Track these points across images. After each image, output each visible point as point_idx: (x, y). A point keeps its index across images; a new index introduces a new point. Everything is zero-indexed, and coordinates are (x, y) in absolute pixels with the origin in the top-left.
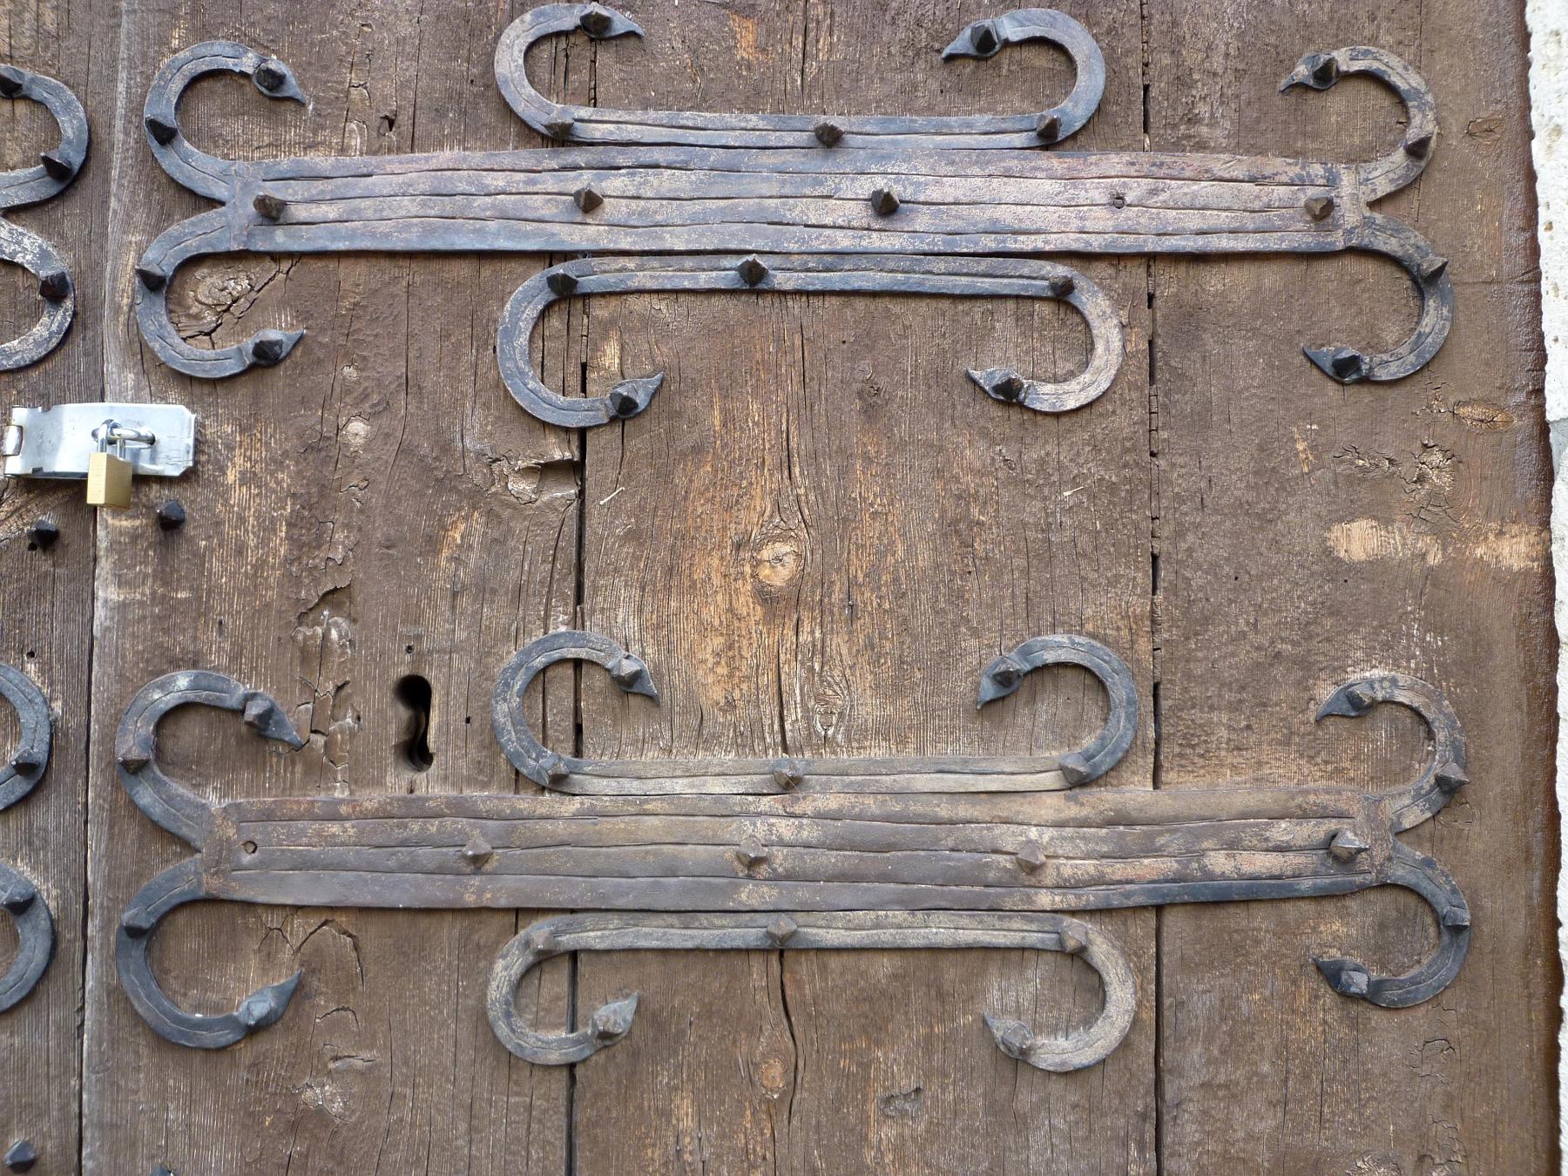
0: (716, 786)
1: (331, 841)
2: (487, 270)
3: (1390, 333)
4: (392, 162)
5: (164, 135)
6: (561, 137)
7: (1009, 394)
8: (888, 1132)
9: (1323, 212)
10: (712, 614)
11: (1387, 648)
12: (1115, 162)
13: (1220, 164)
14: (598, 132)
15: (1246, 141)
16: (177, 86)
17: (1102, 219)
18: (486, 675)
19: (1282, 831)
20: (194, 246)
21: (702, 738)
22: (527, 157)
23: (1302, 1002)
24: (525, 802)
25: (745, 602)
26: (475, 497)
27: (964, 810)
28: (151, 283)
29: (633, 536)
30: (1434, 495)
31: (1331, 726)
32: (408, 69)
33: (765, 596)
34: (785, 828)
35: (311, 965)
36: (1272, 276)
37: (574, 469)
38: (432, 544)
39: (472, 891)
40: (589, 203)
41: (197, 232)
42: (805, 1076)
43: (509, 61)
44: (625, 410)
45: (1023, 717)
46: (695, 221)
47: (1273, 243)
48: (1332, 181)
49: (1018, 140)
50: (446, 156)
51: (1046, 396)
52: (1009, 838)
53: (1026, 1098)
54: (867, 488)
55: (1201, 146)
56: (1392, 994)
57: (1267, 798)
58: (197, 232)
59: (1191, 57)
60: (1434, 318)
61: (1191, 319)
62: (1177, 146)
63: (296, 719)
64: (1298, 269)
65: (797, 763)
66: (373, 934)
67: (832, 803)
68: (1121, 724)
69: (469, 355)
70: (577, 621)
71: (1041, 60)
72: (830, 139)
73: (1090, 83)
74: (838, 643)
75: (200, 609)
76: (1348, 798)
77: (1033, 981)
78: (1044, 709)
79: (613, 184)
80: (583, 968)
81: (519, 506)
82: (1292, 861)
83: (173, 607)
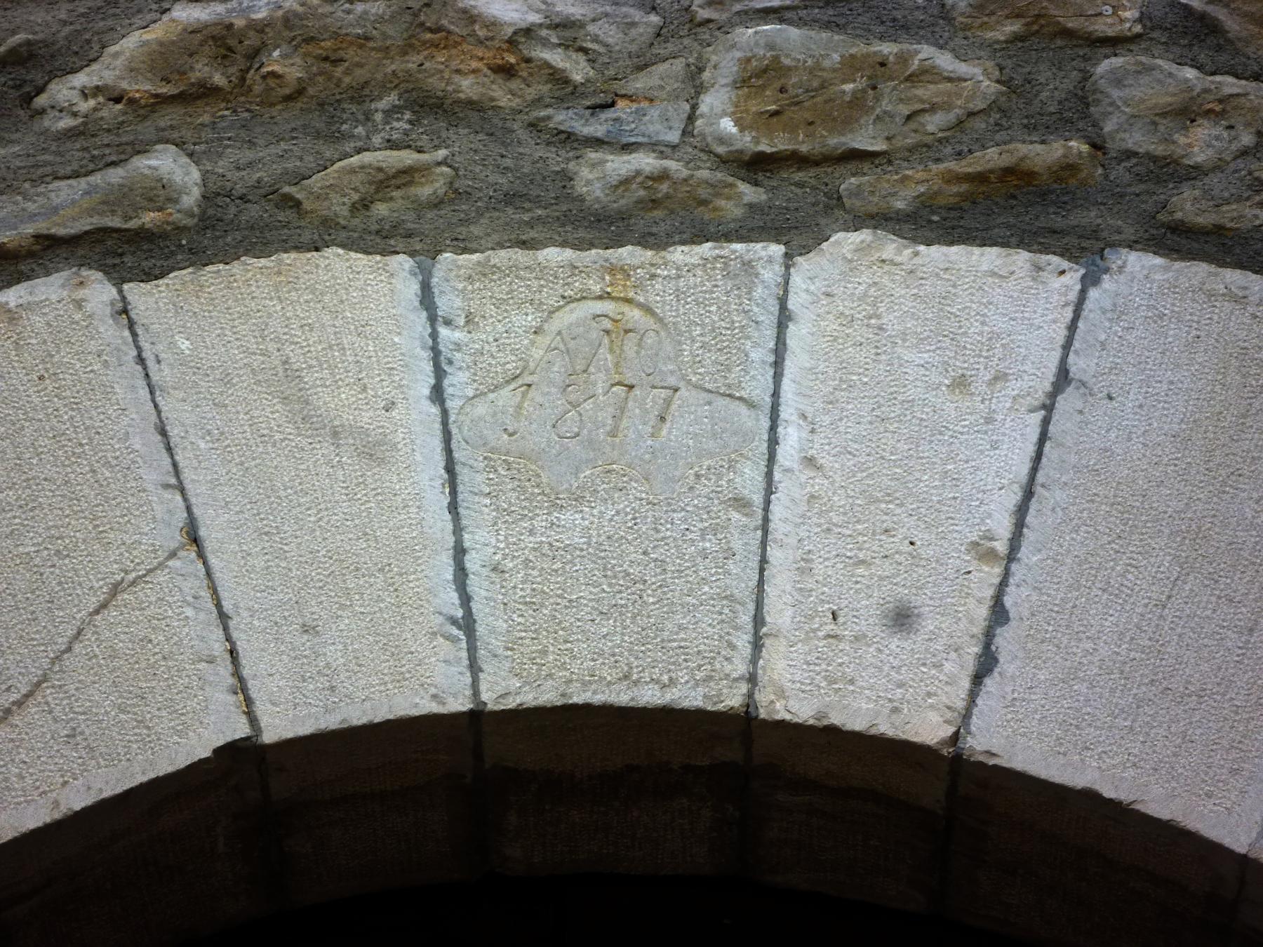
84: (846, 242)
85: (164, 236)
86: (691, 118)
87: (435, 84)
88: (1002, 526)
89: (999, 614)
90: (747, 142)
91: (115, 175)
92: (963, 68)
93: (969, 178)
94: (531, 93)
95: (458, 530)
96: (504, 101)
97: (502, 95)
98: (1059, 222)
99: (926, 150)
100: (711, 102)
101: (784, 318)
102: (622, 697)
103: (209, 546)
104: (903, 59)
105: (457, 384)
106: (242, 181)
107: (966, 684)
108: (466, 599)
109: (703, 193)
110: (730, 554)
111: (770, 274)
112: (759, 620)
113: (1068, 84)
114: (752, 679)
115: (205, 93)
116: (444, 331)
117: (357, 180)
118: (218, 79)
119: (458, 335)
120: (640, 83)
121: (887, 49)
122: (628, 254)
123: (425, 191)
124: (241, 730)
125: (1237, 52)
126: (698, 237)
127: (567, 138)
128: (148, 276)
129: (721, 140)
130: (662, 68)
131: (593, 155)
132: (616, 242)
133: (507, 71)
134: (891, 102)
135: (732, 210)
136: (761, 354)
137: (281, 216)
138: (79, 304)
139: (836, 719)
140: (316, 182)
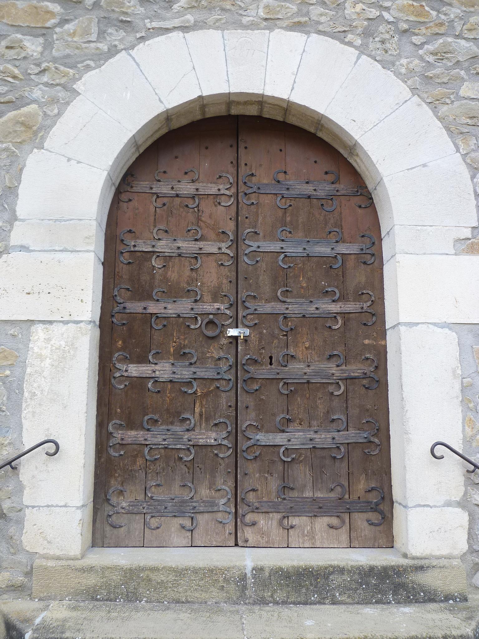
0: (301, 366)
1: (264, 372)
2: (277, 315)
3: (370, 320)
4: (268, 304)
5: (244, 302)
6: (284, 302)
7: (330, 327)
8: (319, 401)
9: (362, 308)
10: (300, 349)
11: (370, 353)
12: (341, 303)
13: (351, 303)
14: (288, 301)
15: (354, 301)
16: (245, 296)
17: (339, 309)
18: (278, 355)
19: (359, 371)
20: (248, 313)
21: (300, 362)
22: (281, 304)
23: (362, 389)
24: (283, 368)
25: (304, 348)
26: (277, 338)
27: (326, 369)
28: (244, 317)
29: (293, 342)
30: (375, 337)
31: (364, 361)
32: (268, 294)
33: (306, 348)
34: (308, 370)
35: (262, 385)
36: (357, 315)
37: (286, 335)
38: (273, 343)
39: (278, 377)
40: (287, 309)
41: (248, 311)
42: (311, 396)
43: (279, 294)
44: (292, 329)
45: (332, 360)
46: (298, 310)
47: (357, 311)
48: (363, 305)
49: (330, 301)
50: (273, 303)
51: (334, 327)
52: (331, 372)
53: (333, 398)
54: (316, 337)
55: (350, 301)
56: (370, 388)
57: (357, 368)
58: (248, 311)
59: (348, 292)
60: (374, 319)
61: (349, 319)
62: (347, 301)
63: (260, 360)
64: (21, 452)
65: (309, 364)
66: (268, 381)
67: (313, 368)
68: (342, 360)
69: (276, 324)
70: (287, 350)
71: (333, 293)
72: (311, 302)
73: (338, 295)
74: (313, 352)
75: (249, 349)
76: (366, 368)
77: (334, 386)
78: (334, 359)
79: (290, 306)
80: (289, 385)
81: (281, 339)
82: (360, 374)
83: (246, 349)
84: (277, 31)
85: (189, 27)
86: (257, 13)
87: (224, 7)
88: (296, 70)
89: (295, 82)
90: (265, 16)
91: (182, 18)
92: (293, 7)
93: (293, 22)
94: (236, 8)
95: (227, 69)
96: (233, 9)
97: (233, 8)
98: (304, 29)
99: (288, 18)
100: (259, 10)
101: (269, 41)
102: (248, 91)
103: (196, 69)
104: (285, 5)
105: (227, 48)
106: (199, 20)
107: (290, 91)
108: (228, 78)
109: (259, 23)
110: (261, 73)
111: (267, 35)
112: (265, 82)
113: (306, 10)
114: (264, 89)
115: (194, 7)
116: (225, 41)
117: (214, 20)
118: (196, 5)
119: (227, 42)
120: (250, 7)
121: (283, 4)
122: (249, 31)
123: (223, 22)
124: (200, 94)
125: (328, 7)
126: (258, 29)
127: (241, 15)
128: (187, 33)
129: (261, 16)
130: (253, 5)
131: (244, 17)
132: (247, 30)
133: (233, 5)
134: (283, 11)
135: (262, 26)
136: (266, 46)
137: (204, 24)
138: (179, 36)
139: (274, 95)
140: (209, 20)
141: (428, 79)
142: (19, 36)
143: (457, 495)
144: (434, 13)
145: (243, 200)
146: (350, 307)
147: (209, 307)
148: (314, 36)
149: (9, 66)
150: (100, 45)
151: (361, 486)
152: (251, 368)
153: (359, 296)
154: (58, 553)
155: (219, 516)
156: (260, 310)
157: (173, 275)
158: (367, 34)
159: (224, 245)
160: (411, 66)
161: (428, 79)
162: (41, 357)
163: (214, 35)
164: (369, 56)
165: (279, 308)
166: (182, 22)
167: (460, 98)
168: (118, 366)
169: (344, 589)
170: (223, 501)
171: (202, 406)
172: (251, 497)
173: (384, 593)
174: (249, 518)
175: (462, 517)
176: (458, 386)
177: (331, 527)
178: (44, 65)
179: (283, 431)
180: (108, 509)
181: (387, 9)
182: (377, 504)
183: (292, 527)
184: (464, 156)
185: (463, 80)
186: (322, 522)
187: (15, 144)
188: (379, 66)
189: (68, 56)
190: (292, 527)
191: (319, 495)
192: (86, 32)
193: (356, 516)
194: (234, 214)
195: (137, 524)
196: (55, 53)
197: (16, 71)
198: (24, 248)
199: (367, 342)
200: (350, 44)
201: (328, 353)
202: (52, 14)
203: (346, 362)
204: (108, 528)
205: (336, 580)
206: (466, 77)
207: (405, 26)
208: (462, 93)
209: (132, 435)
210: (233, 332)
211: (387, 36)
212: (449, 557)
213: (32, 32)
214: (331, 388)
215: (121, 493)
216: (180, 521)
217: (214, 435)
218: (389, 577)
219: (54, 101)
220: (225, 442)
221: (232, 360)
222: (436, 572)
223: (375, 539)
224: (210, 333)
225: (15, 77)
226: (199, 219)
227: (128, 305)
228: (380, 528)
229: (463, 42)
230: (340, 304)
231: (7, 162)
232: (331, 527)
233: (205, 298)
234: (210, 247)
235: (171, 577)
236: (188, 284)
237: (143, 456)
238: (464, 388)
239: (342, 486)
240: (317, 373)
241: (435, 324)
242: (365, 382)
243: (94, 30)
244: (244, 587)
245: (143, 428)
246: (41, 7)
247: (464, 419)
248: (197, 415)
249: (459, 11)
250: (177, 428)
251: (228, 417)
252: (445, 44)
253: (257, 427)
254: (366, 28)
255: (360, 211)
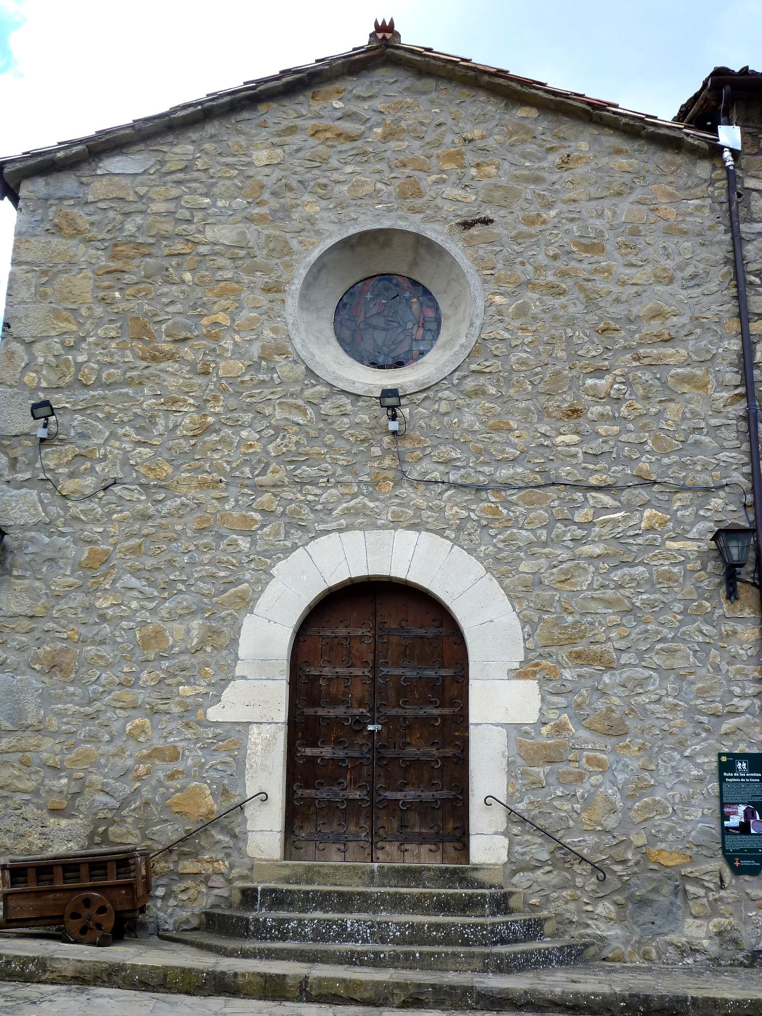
141: (498, 560)
142: (235, 536)
143: (502, 828)
144: (505, 511)
145: (379, 641)
146: (446, 711)
147: (357, 711)
148: (423, 533)
149: (229, 558)
150: (287, 543)
151: (451, 826)
152: (382, 751)
153: (452, 704)
154: (267, 857)
155: (362, 844)
156: (388, 713)
157: (333, 690)
158: (459, 529)
159: (366, 670)
160: (487, 552)
161: (498, 560)
162: (256, 744)
163: (359, 534)
164: (459, 546)
165: (400, 712)
166: (339, 525)
167: (518, 572)
168: (299, 749)
169: (430, 880)
170: (364, 834)
171: (351, 773)
172: (381, 832)
173: (454, 883)
174: (380, 844)
175: (505, 842)
176: (505, 762)
177: (431, 851)
178: (251, 557)
179: (402, 791)
180: (293, 838)
181: (473, 511)
182: (460, 837)
183: (406, 850)
184: (518, 614)
185: (522, 559)
186: (425, 848)
187: (235, 610)
188: (466, 553)
189: (266, 550)
190: (406, 850)
191: (424, 831)
192: (277, 533)
193: (447, 844)
194: (373, 649)
195: (311, 847)
196: (258, 549)
197: (234, 561)
198: (244, 678)
199: (457, 734)
200: (447, 538)
201: (431, 742)
202: (256, 521)
203: (443, 747)
204: (293, 849)
205: (426, 874)
206: (524, 557)
207: (485, 523)
208: (521, 569)
209: (308, 793)
210: (370, 728)
211: (472, 531)
212: (496, 864)
213: (241, 533)
214: (433, 764)
215: (301, 828)
216: (338, 846)
217: (358, 793)
218: (457, 873)
219: (259, 581)
220: (366, 797)
221: (370, 745)
222: (484, 872)
223: (458, 858)
224: (357, 728)
225: (233, 565)
226: (350, 652)
227: (305, 710)
228: (462, 852)
229: (524, 532)
230: (440, 709)
231: (231, 622)
232: (431, 851)
233: (354, 705)
234: (357, 672)
235: (332, 871)
236: (343, 696)
237: (315, 805)
238: (509, 764)
239: (438, 826)
240: (424, 754)
241: (492, 724)
242: (455, 760)
243: (282, 531)
244: (373, 877)
245: (314, 788)
246: (249, 516)
247: (508, 783)
248: (348, 780)
249: (522, 509)
250: (336, 788)
251: (367, 782)
252: (512, 534)
253: (385, 788)
254: (459, 525)
255: (455, 646)
